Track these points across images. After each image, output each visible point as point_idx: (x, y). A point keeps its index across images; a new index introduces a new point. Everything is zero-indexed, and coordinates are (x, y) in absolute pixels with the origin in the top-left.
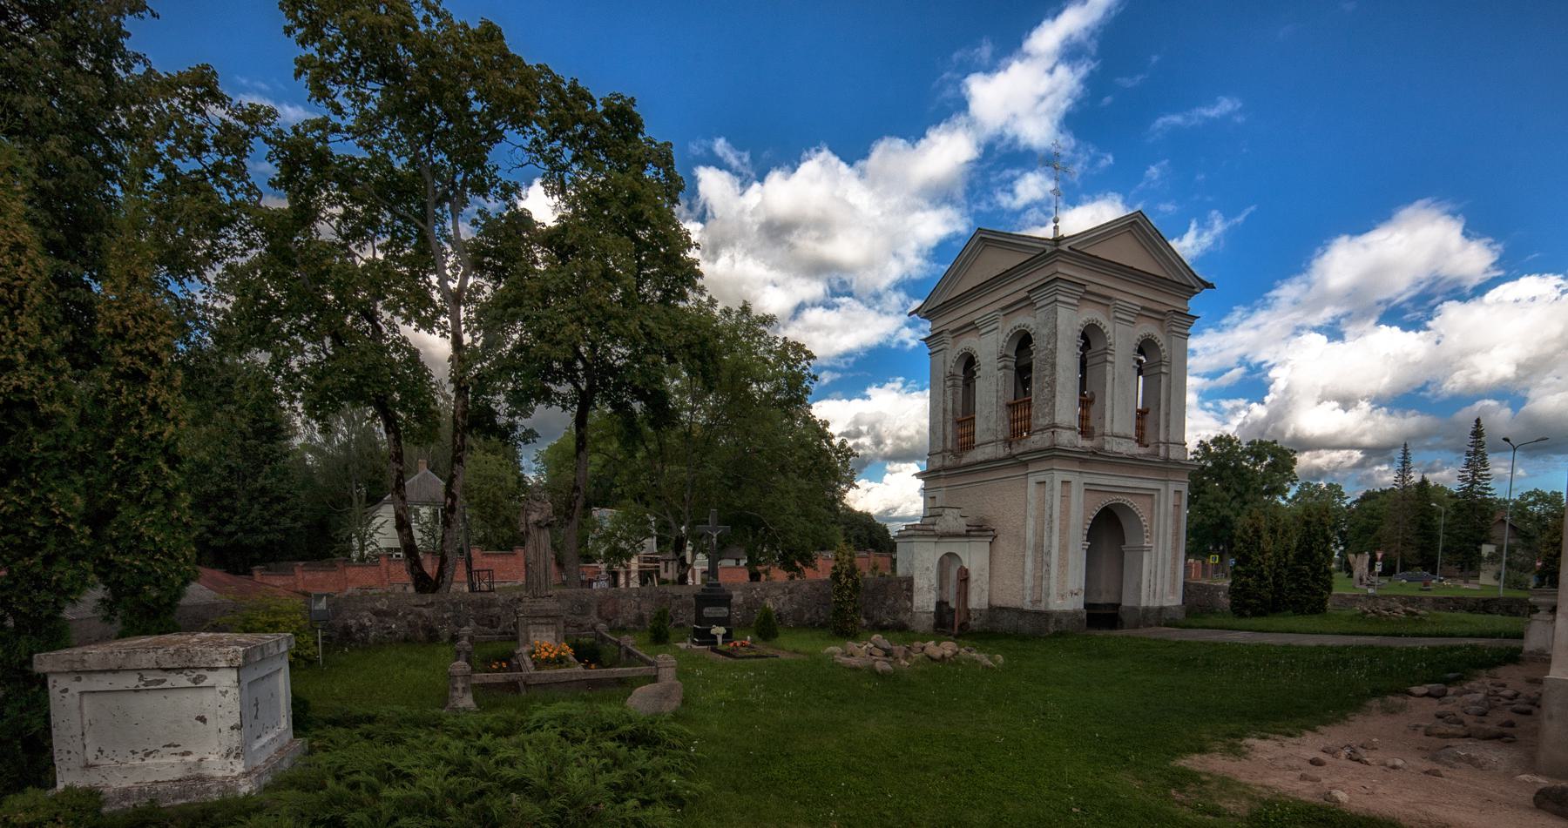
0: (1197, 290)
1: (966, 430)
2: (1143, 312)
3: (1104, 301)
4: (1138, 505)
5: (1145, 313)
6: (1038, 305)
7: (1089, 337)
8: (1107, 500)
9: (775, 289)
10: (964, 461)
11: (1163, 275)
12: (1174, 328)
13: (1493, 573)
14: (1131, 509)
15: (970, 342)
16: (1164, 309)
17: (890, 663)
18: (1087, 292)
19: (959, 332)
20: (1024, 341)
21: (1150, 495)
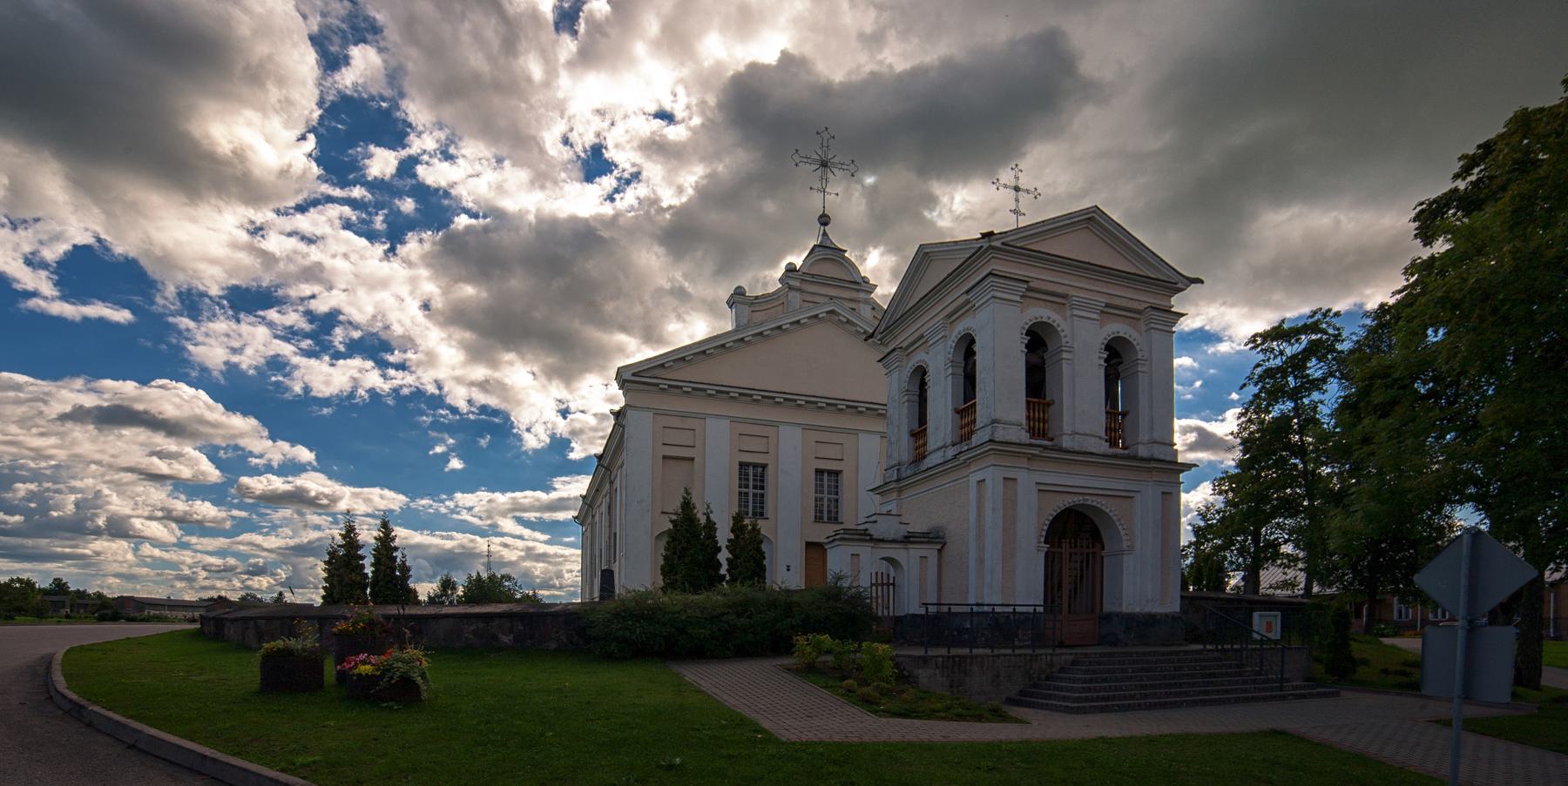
0: (1179, 285)
1: (921, 442)
2: (1106, 310)
3: (1059, 299)
4: (1109, 507)
5: (1110, 311)
6: (977, 306)
7: (1038, 341)
8: (1069, 501)
9: (267, 144)
10: (923, 467)
11: (1133, 270)
12: (1153, 325)
13: (668, 107)
14: (1101, 510)
15: (919, 357)
16: (1141, 307)
17: (188, 505)
18: (1030, 289)
19: (908, 350)
20: (967, 347)
21: (1127, 497)
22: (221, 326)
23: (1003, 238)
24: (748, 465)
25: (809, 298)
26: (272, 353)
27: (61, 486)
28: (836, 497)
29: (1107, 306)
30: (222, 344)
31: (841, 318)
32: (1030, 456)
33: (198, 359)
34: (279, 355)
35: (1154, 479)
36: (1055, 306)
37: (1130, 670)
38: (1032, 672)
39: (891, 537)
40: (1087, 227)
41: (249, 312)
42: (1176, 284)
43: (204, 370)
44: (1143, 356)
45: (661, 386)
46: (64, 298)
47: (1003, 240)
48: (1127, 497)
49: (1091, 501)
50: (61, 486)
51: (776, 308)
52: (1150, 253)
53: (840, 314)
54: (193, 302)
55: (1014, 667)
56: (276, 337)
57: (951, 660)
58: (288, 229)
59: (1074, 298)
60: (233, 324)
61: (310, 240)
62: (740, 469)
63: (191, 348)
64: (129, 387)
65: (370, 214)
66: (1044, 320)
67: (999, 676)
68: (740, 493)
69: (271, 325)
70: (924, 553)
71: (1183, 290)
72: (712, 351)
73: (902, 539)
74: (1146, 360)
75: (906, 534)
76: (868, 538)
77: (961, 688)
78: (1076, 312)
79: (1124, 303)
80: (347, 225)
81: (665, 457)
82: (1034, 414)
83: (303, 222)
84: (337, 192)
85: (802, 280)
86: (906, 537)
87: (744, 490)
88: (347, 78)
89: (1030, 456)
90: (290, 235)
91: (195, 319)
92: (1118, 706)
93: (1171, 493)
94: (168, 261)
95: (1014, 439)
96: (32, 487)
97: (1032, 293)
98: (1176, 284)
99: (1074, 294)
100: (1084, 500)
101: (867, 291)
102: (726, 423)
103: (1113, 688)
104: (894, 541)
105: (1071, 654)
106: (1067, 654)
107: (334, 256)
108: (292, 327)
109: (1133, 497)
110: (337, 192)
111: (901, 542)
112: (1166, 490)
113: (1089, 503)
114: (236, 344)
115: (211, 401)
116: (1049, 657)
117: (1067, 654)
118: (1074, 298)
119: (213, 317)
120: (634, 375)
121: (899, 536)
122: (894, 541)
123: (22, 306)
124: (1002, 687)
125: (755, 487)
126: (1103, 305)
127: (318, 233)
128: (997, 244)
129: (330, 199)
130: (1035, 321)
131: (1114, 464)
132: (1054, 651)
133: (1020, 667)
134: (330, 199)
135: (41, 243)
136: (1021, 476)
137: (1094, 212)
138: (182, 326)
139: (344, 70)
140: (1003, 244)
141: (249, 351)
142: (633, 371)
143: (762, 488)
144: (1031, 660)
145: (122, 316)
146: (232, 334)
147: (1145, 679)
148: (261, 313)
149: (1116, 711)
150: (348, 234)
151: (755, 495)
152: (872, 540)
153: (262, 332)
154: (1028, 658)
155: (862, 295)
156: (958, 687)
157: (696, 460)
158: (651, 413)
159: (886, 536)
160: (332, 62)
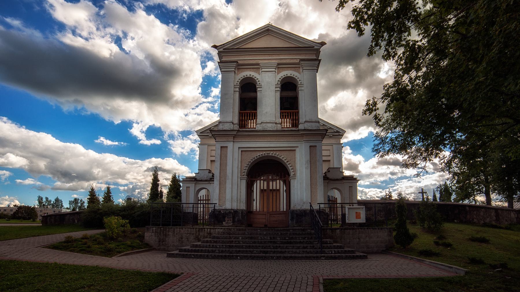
3: (256, 67)
5: (280, 67)
16: (298, 61)
22: (180, 142)
26: (191, 148)
27: (145, 190)
29: (279, 64)
30: (180, 147)
32: (234, 135)
33: (175, 152)
34: (193, 148)
36: (255, 70)
37: (240, 238)
38: (199, 237)
39: (205, 179)
40: (268, 34)
41: (186, 137)
43: (176, 155)
44: (301, 83)
46: (147, 140)
47: (224, 48)
48: (292, 150)
50: (145, 190)
54: (172, 137)
55: (190, 234)
56: (192, 143)
57: (159, 229)
58: (194, 113)
59: (261, 64)
60: (182, 141)
61: (198, 115)
63: (173, 149)
64: (159, 160)
65: (214, 104)
66: (248, 76)
67: (182, 238)
69: (190, 139)
74: (303, 84)
77: (164, 243)
78: (263, 70)
80: (208, 109)
82: (245, 118)
83: (197, 110)
84: (205, 100)
88: (207, 71)
89: (234, 135)
90: (195, 114)
91: (173, 140)
92: (194, 255)
93: (316, 146)
94: (167, 126)
95: (227, 129)
96: (139, 190)
98: (314, 47)
99: (260, 62)
103: (211, 246)
104: (206, 181)
105: (221, 229)
106: (219, 228)
107: (205, 118)
108: (195, 140)
109: (295, 150)
110: (205, 100)
112: (312, 144)
113: (271, 155)
114: (183, 146)
115: (178, 163)
116: (209, 230)
117: (219, 228)
118: (261, 64)
119: (177, 140)
120: (201, 133)
121: (208, 179)
122: (206, 181)
123: (139, 143)
124: (184, 244)
126: (276, 64)
127: (201, 113)
129: (204, 102)
131: (281, 135)
132: (203, 226)
133: (193, 234)
134: (204, 102)
135: (143, 126)
136: (230, 145)
137: (268, 27)
138: (171, 143)
139: (206, 68)
140: (223, 49)
141: (186, 148)
144: (199, 231)
145: (158, 142)
146: (182, 144)
147: (241, 243)
148: (188, 137)
149: (192, 258)
150: (209, 112)
153: (189, 141)
154: (197, 230)
156: (162, 242)
159: (203, 179)
160: (204, 67)
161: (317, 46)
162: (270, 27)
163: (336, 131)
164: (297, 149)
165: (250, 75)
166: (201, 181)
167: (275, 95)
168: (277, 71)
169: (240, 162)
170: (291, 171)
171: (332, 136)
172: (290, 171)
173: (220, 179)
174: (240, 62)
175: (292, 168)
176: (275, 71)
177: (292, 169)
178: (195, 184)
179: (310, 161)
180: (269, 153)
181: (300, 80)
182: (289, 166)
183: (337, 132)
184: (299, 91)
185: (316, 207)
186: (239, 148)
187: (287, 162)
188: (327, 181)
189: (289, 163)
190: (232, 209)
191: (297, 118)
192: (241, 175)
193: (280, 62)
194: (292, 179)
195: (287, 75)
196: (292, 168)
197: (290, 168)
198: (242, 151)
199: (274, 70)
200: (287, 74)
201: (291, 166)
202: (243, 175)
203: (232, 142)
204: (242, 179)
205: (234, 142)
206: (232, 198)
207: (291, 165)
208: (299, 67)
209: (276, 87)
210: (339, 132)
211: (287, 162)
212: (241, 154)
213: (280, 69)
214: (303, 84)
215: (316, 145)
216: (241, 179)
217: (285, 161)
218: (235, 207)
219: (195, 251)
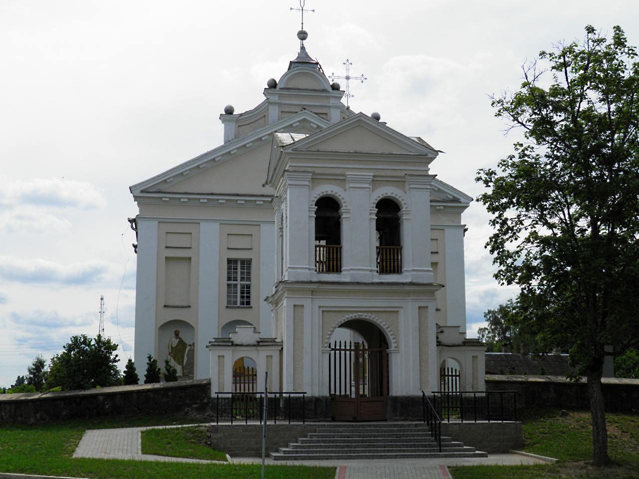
3: (341, 179)
16: (402, 174)
23: (292, 146)
24: (236, 261)
25: (287, 110)
28: (230, 282)
31: (312, 125)
35: (411, 298)
36: (338, 182)
42: (427, 155)
44: (406, 208)
45: (164, 199)
49: (364, 316)
51: (259, 121)
52: (403, 137)
53: (311, 122)
62: (228, 263)
68: (229, 285)
70: (269, 353)
71: (435, 158)
72: (204, 165)
73: (256, 343)
75: (259, 340)
76: (230, 344)
79: (388, 173)
81: (167, 258)
85: (280, 94)
86: (258, 342)
87: (232, 282)
93: (427, 307)
97: (316, 178)
100: (359, 315)
101: (337, 97)
102: (216, 226)
109: (398, 311)
111: (254, 345)
120: (142, 192)
121: (253, 341)
125: (242, 279)
128: (290, 151)
130: (321, 195)
136: (307, 302)
137: (360, 116)
142: (141, 189)
143: (249, 279)
151: (243, 287)
152: (233, 345)
155: (332, 102)
157: (192, 260)
158: (157, 222)
161: (431, 153)
162: (362, 117)
163: (451, 198)
164: (401, 312)
165: (332, 191)
166: (242, 345)
167: (370, 224)
168: (371, 187)
169: (321, 328)
170: (392, 341)
171: (442, 208)
172: (388, 335)
173: (294, 353)
174: (318, 171)
175: (395, 341)
176: (369, 188)
177: (395, 342)
178: (233, 351)
179: (419, 329)
180: (362, 315)
181: (405, 204)
182: (389, 334)
183: (456, 200)
184: (404, 221)
185: (428, 393)
186: (320, 307)
187: (387, 328)
188: (440, 348)
189: (389, 329)
190: (312, 397)
191: (399, 258)
192: (322, 347)
193: (376, 174)
194: (393, 353)
195: (386, 194)
196: (394, 337)
197: (391, 337)
198: (323, 311)
199: (367, 186)
200: (386, 192)
201: (392, 335)
202: (326, 347)
203: (310, 299)
204: (324, 353)
205: (312, 298)
206: (312, 382)
207: (392, 333)
208: (405, 182)
209: (370, 214)
210: (457, 201)
211: (387, 328)
212: (322, 315)
213: (375, 182)
214: (409, 211)
215: (427, 305)
216: (323, 353)
217: (385, 327)
218: (316, 394)
219: (297, 452)
